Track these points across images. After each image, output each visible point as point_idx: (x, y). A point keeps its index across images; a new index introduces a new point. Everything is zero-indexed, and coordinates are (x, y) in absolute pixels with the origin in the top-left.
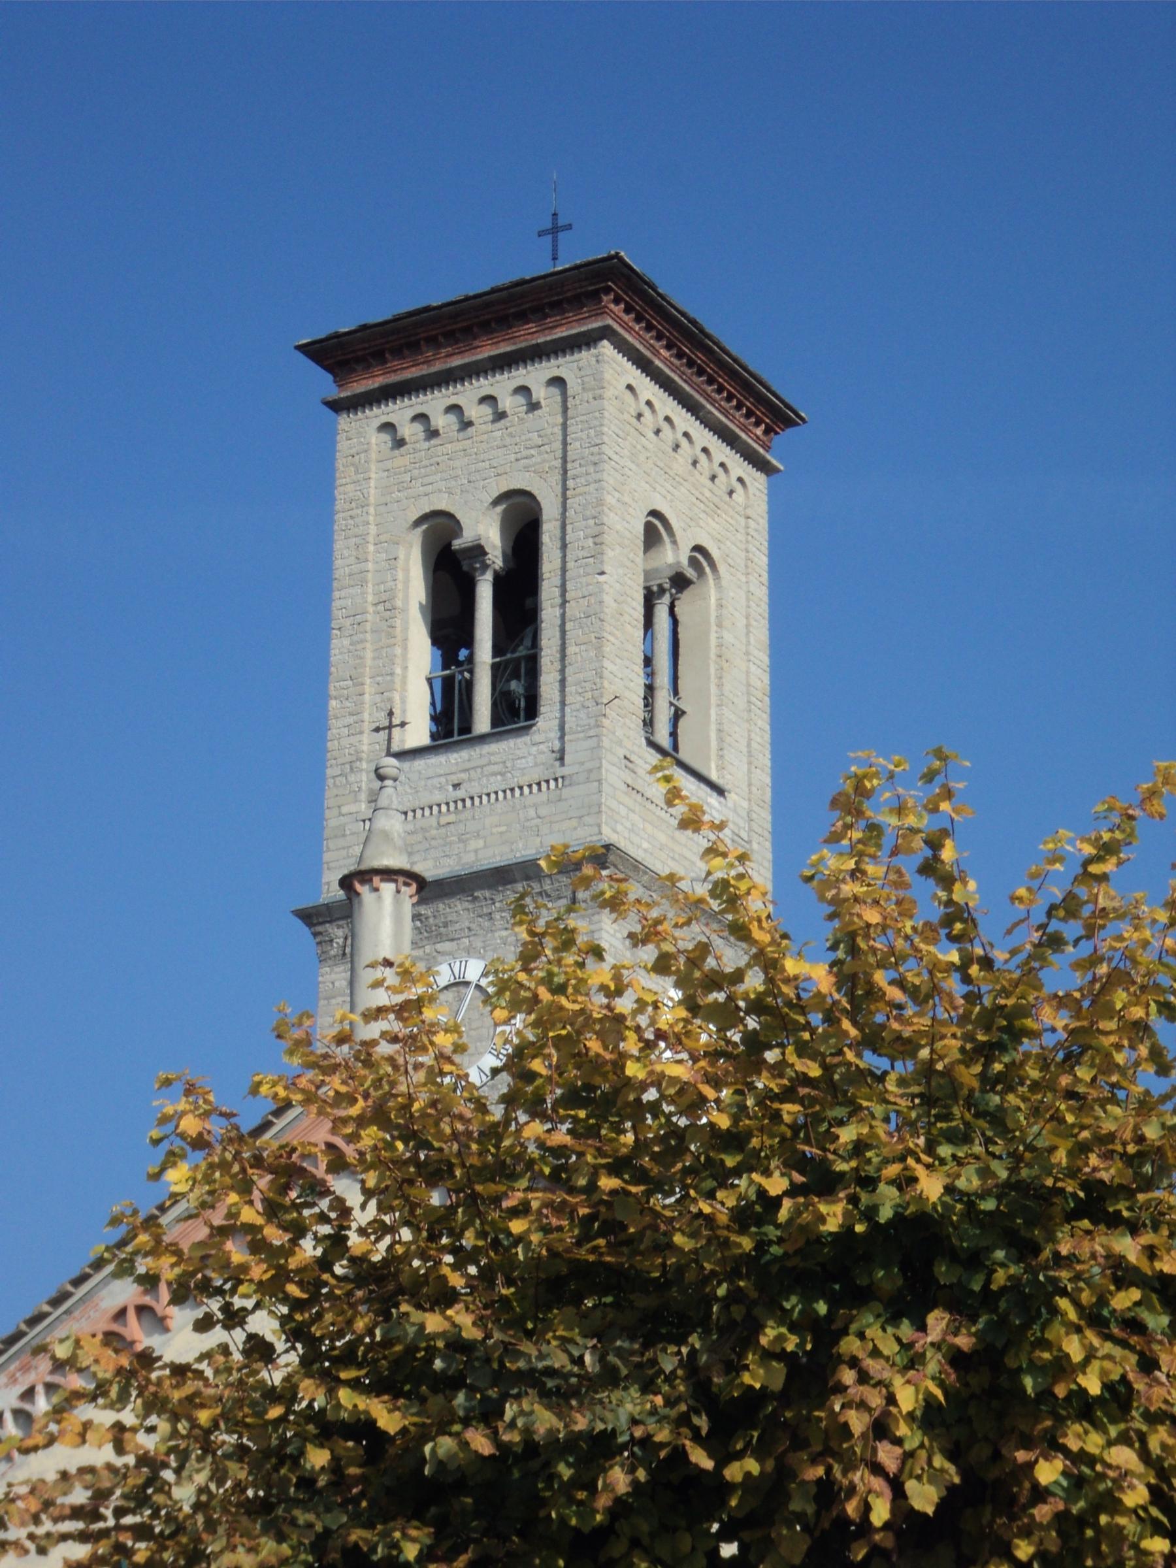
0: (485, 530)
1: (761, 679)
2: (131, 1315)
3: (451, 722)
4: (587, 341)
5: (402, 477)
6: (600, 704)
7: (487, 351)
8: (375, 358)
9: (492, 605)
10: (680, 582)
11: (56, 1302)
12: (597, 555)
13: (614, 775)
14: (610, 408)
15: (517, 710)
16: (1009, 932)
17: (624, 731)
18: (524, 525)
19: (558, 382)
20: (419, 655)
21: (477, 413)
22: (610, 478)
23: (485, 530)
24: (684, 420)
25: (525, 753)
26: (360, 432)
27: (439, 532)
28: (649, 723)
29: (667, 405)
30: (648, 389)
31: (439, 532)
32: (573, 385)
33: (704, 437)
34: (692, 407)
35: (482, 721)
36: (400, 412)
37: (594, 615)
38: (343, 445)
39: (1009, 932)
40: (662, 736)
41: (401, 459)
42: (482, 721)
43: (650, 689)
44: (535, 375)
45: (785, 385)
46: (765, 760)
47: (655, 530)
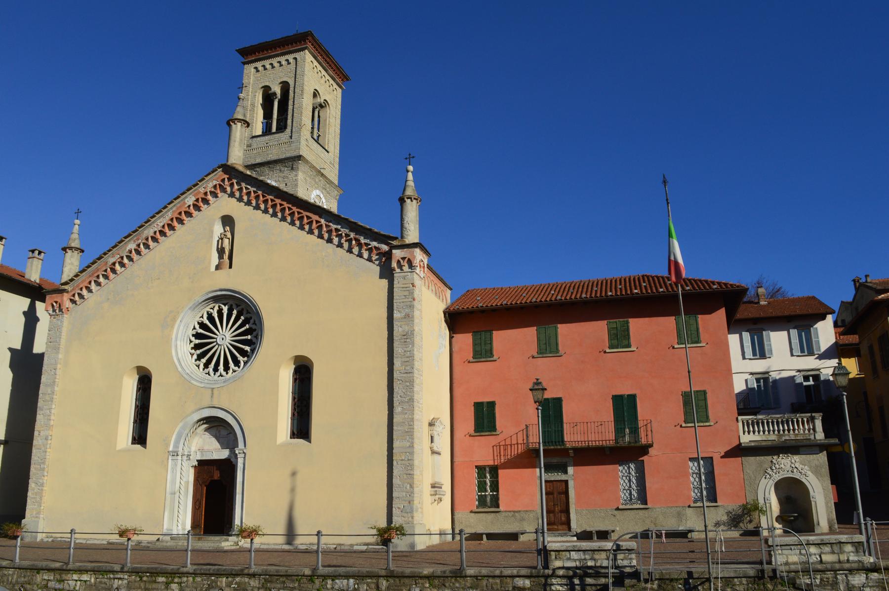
0: (277, 89)
1: (338, 131)
2: (166, 227)
3: (267, 131)
4: (303, 50)
5: (257, 78)
6: (301, 127)
7: (290, 107)
8: (254, 52)
9: (278, 107)
10: (321, 106)
11: (146, 222)
12: (302, 95)
13: (303, 142)
14: (307, 65)
15: (282, 127)
16: (303, 373)
17: (306, 133)
18: (285, 86)
19: (295, 59)
20: (260, 113)
21: (276, 65)
22: (306, 79)
23: (277, 89)
24: (324, 72)
25: (284, 136)
26: (249, 69)
27: (266, 89)
28: (312, 133)
29: (320, 68)
30: (316, 63)
31: (266, 89)
32: (299, 59)
33: (328, 77)
34: (326, 70)
35: (274, 129)
36: (259, 65)
37: (301, 107)
38: (245, 71)
39: (303, 373)
40: (315, 137)
41: (258, 74)
42: (274, 129)
43: (313, 128)
44: (290, 57)
45: (347, 71)
46: (338, 148)
47: (316, 94)
